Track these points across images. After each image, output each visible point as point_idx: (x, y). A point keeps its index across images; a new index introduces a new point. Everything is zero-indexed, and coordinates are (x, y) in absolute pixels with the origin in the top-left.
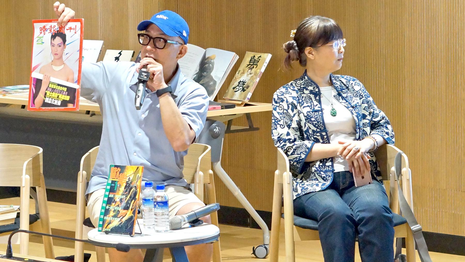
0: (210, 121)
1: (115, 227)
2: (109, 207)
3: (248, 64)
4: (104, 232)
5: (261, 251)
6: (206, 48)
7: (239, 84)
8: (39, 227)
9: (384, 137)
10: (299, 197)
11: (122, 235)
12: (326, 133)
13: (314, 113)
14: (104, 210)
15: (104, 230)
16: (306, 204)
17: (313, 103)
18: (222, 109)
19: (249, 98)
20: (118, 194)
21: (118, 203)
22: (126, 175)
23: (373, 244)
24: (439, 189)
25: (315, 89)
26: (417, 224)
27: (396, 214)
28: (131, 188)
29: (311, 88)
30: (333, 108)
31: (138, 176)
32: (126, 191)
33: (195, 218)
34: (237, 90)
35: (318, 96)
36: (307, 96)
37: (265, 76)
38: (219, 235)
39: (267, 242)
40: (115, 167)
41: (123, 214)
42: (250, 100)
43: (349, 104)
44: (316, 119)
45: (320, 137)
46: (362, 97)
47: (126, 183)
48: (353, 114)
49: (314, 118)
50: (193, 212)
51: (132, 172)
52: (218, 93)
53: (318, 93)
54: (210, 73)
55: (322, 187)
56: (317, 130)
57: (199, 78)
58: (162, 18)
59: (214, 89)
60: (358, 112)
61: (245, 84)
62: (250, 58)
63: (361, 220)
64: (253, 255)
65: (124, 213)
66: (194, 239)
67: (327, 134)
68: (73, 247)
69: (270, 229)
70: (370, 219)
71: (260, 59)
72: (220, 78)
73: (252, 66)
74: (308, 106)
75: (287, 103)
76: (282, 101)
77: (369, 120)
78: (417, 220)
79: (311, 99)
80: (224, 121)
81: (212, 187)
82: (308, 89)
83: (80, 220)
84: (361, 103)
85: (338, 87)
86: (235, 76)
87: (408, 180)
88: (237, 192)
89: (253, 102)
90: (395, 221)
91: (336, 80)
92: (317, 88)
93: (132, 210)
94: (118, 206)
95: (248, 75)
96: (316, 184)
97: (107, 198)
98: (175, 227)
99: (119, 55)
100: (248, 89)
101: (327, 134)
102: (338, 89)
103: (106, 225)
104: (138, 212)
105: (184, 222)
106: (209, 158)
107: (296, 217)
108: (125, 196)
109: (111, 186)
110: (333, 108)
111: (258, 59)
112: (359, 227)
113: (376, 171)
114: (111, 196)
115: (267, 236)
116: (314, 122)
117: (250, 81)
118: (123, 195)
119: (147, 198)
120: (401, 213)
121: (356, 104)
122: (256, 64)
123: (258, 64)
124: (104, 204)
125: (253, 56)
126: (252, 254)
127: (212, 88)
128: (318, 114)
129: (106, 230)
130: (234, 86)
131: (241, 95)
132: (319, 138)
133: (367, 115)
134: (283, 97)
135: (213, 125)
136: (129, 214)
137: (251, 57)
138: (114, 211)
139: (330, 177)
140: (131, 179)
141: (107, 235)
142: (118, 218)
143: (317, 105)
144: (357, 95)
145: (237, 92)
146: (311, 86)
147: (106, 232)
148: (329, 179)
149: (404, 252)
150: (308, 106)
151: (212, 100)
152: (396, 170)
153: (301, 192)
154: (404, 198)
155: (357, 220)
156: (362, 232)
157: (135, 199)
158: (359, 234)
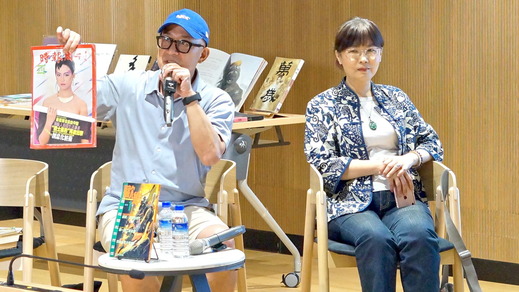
0: (236, 134)
3: (278, 70)
4: (116, 257)
5: (291, 279)
7: (268, 93)
9: (432, 153)
10: (334, 220)
12: (365, 148)
14: (117, 233)
15: (117, 255)
16: (341, 227)
17: (351, 115)
18: (248, 121)
19: (279, 108)
20: (132, 215)
21: (132, 225)
22: (142, 193)
25: (354, 99)
26: (465, 249)
27: (443, 239)
28: (147, 209)
29: (349, 98)
30: (371, 121)
31: (155, 195)
32: (141, 212)
34: (266, 100)
36: (345, 106)
37: (297, 85)
40: (128, 185)
41: (138, 237)
42: (280, 111)
43: (391, 117)
46: (406, 109)
48: (395, 128)
49: (352, 131)
50: (216, 236)
51: (148, 190)
52: (244, 104)
54: (236, 82)
55: (359, 209)
56: (354, 144)
60: (401, 126)
62: (281, 64)
64: (283, 284)
65: (139, 236)
66: (216, 265)
67: (365, 150)
68: (82, 274)
69: (301, 255)
70: (413, 244)
71: (291, 66)
72: (247, 86)
73: (282, 74)
74: (346, 118)
75: (322, 114)
80: (251, 135)
81: (237, 208)
82: (346, 98)
83: (89, 244)
85: (379, 98)
86: (263, 84)
91: (377, 90)
93: (147, 232)
94: (132, 228)
95: (277, 83)
97: (120, 220)
98: (196, 252)
99: (134, 60)
100: (278, 98)
101: (365, 150)
103: (118, 250)
104: (154, 235)
105: (206, 247)
106: (234, 175)
108: (139, 218)
109: (124, 206)
110: (371, 121)
111: (289, 65)
112: (400, 253)
114: (125, 217)
115: (298, 263)
116: (352, 136)
118: (138, 216)
120: (447, 236)
121: (399, 118)
123: (288, 71)
125: (284, 62)
126: (281, 283)
127: (237, 98)
128: (356, 127)
129: (118, 255)
130: (262, 96)
131: (269, 105)
132: (357, 153)
133: (411, 129)
134: (317, 107)
135: (239, 138)
136: (144, 237)
137: (282, 63)
138: (127, 234)
139: (369, 196)
141: (120, 260)
142: (132, 241)
143: (355, 117)
146: (349, 96)
147: (118, 257)
148: (367, 199)
149: (451, 280)
150: (346, 118)
151: (238, 111)
155: (398, 245)
157: (151, 221)
158: (401, 261)
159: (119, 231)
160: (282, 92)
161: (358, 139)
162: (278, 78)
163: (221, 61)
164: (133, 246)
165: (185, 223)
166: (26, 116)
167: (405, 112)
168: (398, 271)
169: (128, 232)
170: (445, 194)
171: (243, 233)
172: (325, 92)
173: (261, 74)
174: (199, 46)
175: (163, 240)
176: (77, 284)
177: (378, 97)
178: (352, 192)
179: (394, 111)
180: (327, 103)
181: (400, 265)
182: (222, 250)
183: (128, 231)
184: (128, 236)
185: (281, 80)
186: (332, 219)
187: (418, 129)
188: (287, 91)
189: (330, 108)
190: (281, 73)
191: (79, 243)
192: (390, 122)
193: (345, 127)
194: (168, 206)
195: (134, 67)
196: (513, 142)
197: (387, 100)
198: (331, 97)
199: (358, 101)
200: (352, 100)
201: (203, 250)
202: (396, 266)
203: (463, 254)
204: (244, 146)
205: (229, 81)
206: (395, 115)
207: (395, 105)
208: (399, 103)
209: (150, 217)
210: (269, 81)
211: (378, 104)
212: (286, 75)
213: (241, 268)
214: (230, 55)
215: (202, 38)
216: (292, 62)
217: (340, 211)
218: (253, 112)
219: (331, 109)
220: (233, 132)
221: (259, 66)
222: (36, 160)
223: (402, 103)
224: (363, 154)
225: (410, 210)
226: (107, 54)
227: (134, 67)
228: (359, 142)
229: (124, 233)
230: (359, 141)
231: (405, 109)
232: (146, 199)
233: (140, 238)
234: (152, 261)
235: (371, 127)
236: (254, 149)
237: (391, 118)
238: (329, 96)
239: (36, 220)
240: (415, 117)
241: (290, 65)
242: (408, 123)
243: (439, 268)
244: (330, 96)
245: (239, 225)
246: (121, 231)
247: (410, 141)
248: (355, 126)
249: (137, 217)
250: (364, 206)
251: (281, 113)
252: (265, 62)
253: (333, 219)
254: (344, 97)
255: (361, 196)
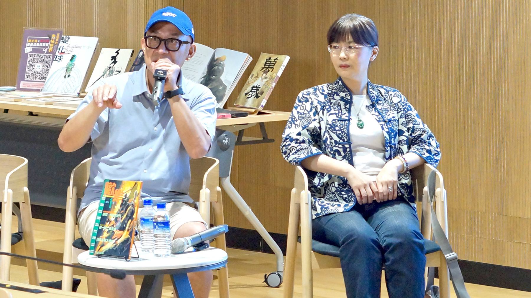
1: (109, 250)
2: (103, 227)
4: (96, 255)
5: (274, 279)
6: (215, 49)
7: (253, 89)
8: (22, 250)
9: (423, 155)
10: (319, 218)
11: (117, 259)
13: (340, 121)
15: (96, 253)
16: (325, 227)
17: (341, 111)
18: (232, 117)
19: (264, 105)
20: (113, 212)
21: (113, 222)
22: (123, 190)
23: (401, 274)
24: (478, 212)
25: (347, 96)
26: (452, 251)
27: (429, 240)
28: (128, 206)
29: (342, 94)
30: (359, 119)
31: (136, 192)
32: (122, 209)
33: (199, 241)
34: (250, 96)
35: (349, 104)
36: (337, 102)
37: (282, 81)
38: (227, 261)
39: (281, 269)
40: (109, 182)
41: (118, 235)
42: (265, 108)
43: (381, 118)
44: (340, 128)
45: (342, 149)
46: (400, 111)
47: (123, 201)
48: (383, 129)
49: (339, 127)
50: (198, 235)
51: (129, 188)
52: (227, 100)
53: (349, 101)
55: (345, 208)
56: (339, 141)
57: (207, 81)
58: (170, 15)
59: (225, 95)
60: (390, 128)
61: (258, 90)
62: (266, 60)
63: (388, 246)
64: (265, 283)
65: (119, 234)
66: (198, 264)
67: (350, 147)
68: (61, 271)
69: (284, 254)
73: (267, 70)
74: (335, 114)
75: (311, 105)
76: (307, 101)
77: (406, 137)
78: (451, 247)
79: (340, 106)
81: (219, 209)
82: (340, 94)
84: (399, 118)
85: (374, 97)
86: (248, 80)
87: (443, 202)
88: (248, 211)
89: (267, 110)
90: (427, 248)
91: (373, 89)
92: (349, 96)
93: (128, 231)
95: (262, 79)
96: (337, 204)
98: (177, 251)
99: (116, 54)
100: (263, 95)
102: (373, 99)
103: (98, 247)
104: (135, 233)
105: (188, 246)
106: (217, 174)
107: (314, 241)
108: (120, 215)
109: (105, 204)
110: (359, 119)
111: (274, 61)
112: (385, 254)
113: (410, 196)
114: (105, 214)
115: (281, 262)
117: (265, 86)
118: (119, 213)
119: (145, 218)
120: (433, 238)
121: (391, 119)
122: (272, 67)
123: (274, 67)
124: (96, 224)
125: (269, 58)
126: (263, 282)
127: (221, 94)
129: (98, 253)
130: (246, 92)
131: (253, 102)
132: (341, 150)
133: (404, 131)
134: (308, 97)
135: (222, 135)
136: (125, 235)
138: (108, 231)
139: (353, 197)
140: (128, 196)
142: (112, 239)
143: (345, 114)
144: (394, 108)
145: (249, 99)
146: (343, 92)
147: (98, 256)
148: (351, 200)
149: (436, 282)
151: (222, 108)
152: (429, 190)
153: (321, 212)
154: (438, 222)
155: (383, 246)
156: (389, 261)
158: (386, 262)
159: (99, 228)
160: (267, 89)
161: (344, 135)
162: (263, 74)
163: (205, 56)
164: (114, 244)
165: (167, 221)
166: (5, 110)
167: (400, 113)
168: (383, 272)
169: (108, 230)
170: (431, 195)
171: (226, 232)
172: (320, 86)
173: (246, 70)
174: (187, 43)
175: (144, 238)
176: (55, 281)
177: (372, 96)
178: (335, 193)
179: (387, 111)
180: (318, 96)
181: (385, 267)
182: (204, 250)
183: (109, 228)
184: (109, 234)
185: (266, 76)
186: (317, 216)
187: (411, 130)
188: (272, 88)
189: (319, 102)
190: (266, 69)
191: (59, 239)
192: (379, 122)
193: (333, 123)
194: (150, 204)
195: (116, 60)
196: (502, 142)
197: (382, 100)
198: (324, 92)
199: (351, 98)
200: (345, 97)
201: (185, 249)
202: (381, 268)
203: (449, 256)
204: (227, 143)
205: (212, 77)
206: (387, 115)
207: (389, 106)
208: (394, 104)
209: (131, 215)
210: (254, 77)
211: (371, 103)
212: (271, 71)
213: (223, 267)
214: (214, 50)
215: (190, 34)
216: (278, 58)
217: (324, 209)
218: (238, 108)
219: (320, 103)
220: (218, 129)
221: (244, 61)
222: (18, 156)
223: (396, 104)
224: (348, 151)
225: (395, 211)
226: (89, 47)
227: (116, 60)
228: (344, 139)
229: (104, 230)
230: (345, 138)
231: (399, 110)
232: (128, 197)
233: (121, 236)
234: (132, 260)
235: (358, 125)
236: (237, 146)
237: (381, 119)
238: (322, 90)
239: (15, 215)
240: (409, 119)
241: (275, 61)
242: (402, 124)
243: (424, 270)
244: (323, 91)
245: (221, 224)
246: (101, 228)
247: (403, 143)
248: (343, 123)
249: (118, 215)
250: (349, 206)
251: (265, 110)
252: (250, 58)
253: (318, 218)
254: (338, 92)
255: (345, 197)
